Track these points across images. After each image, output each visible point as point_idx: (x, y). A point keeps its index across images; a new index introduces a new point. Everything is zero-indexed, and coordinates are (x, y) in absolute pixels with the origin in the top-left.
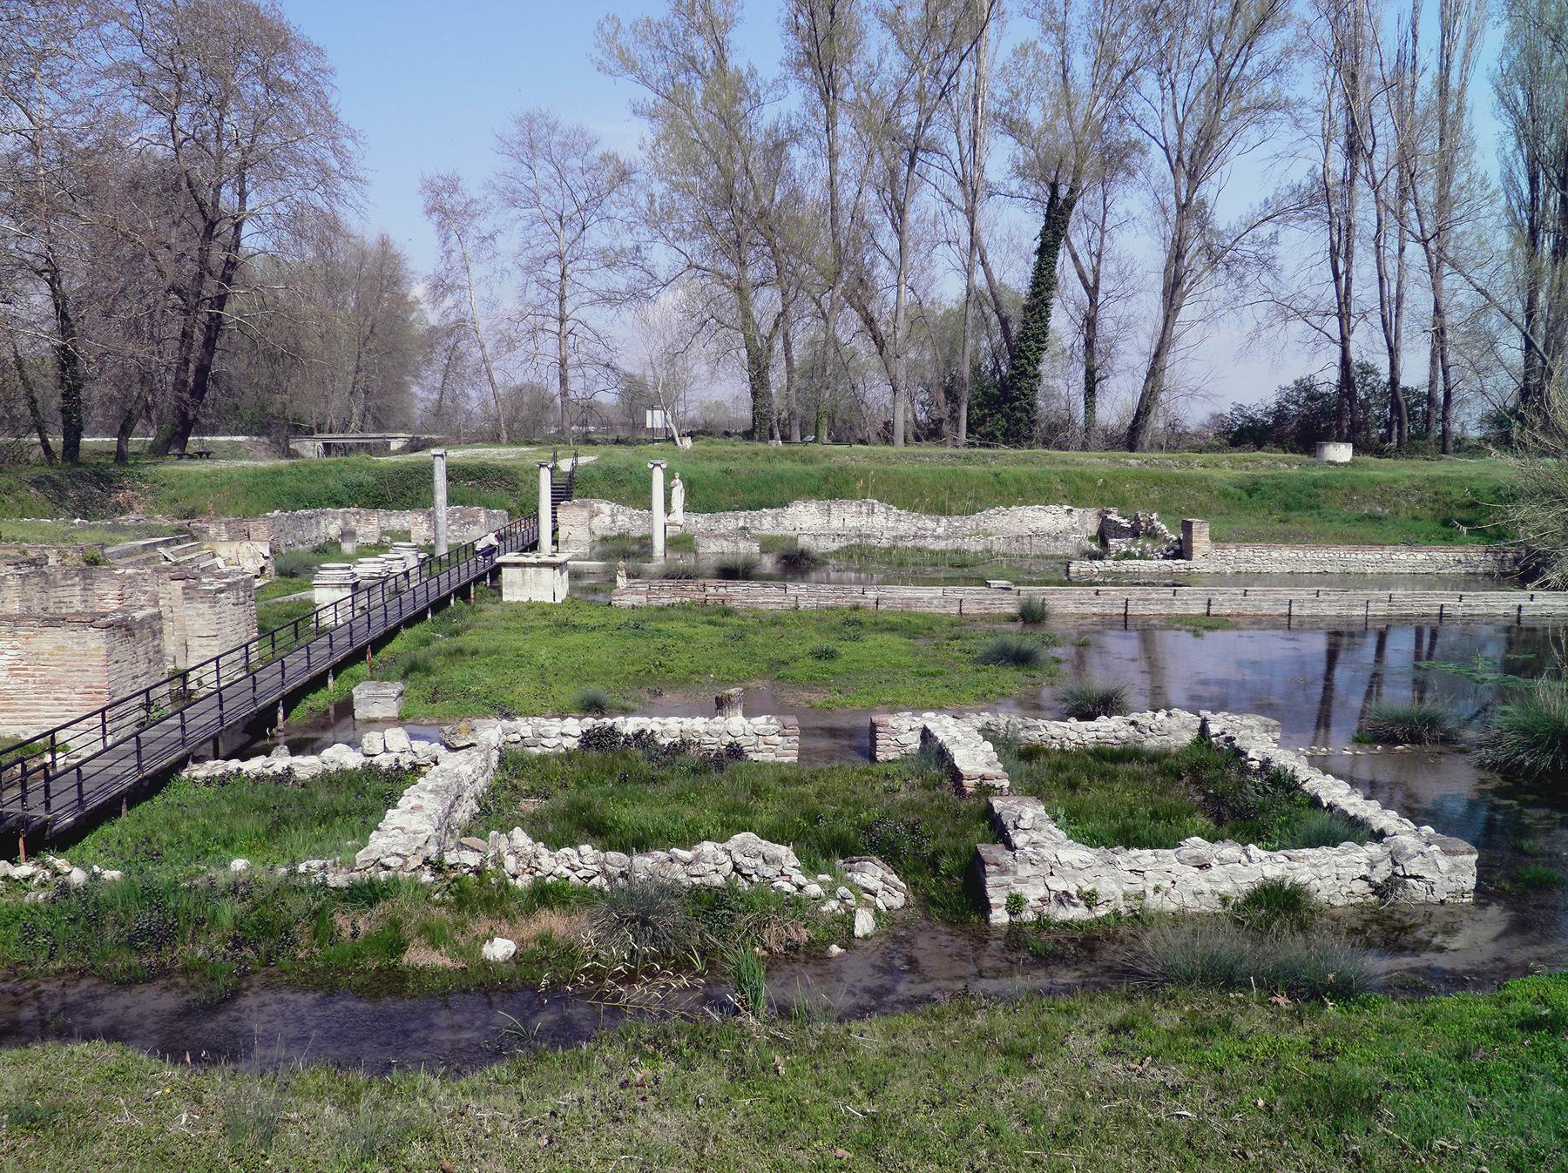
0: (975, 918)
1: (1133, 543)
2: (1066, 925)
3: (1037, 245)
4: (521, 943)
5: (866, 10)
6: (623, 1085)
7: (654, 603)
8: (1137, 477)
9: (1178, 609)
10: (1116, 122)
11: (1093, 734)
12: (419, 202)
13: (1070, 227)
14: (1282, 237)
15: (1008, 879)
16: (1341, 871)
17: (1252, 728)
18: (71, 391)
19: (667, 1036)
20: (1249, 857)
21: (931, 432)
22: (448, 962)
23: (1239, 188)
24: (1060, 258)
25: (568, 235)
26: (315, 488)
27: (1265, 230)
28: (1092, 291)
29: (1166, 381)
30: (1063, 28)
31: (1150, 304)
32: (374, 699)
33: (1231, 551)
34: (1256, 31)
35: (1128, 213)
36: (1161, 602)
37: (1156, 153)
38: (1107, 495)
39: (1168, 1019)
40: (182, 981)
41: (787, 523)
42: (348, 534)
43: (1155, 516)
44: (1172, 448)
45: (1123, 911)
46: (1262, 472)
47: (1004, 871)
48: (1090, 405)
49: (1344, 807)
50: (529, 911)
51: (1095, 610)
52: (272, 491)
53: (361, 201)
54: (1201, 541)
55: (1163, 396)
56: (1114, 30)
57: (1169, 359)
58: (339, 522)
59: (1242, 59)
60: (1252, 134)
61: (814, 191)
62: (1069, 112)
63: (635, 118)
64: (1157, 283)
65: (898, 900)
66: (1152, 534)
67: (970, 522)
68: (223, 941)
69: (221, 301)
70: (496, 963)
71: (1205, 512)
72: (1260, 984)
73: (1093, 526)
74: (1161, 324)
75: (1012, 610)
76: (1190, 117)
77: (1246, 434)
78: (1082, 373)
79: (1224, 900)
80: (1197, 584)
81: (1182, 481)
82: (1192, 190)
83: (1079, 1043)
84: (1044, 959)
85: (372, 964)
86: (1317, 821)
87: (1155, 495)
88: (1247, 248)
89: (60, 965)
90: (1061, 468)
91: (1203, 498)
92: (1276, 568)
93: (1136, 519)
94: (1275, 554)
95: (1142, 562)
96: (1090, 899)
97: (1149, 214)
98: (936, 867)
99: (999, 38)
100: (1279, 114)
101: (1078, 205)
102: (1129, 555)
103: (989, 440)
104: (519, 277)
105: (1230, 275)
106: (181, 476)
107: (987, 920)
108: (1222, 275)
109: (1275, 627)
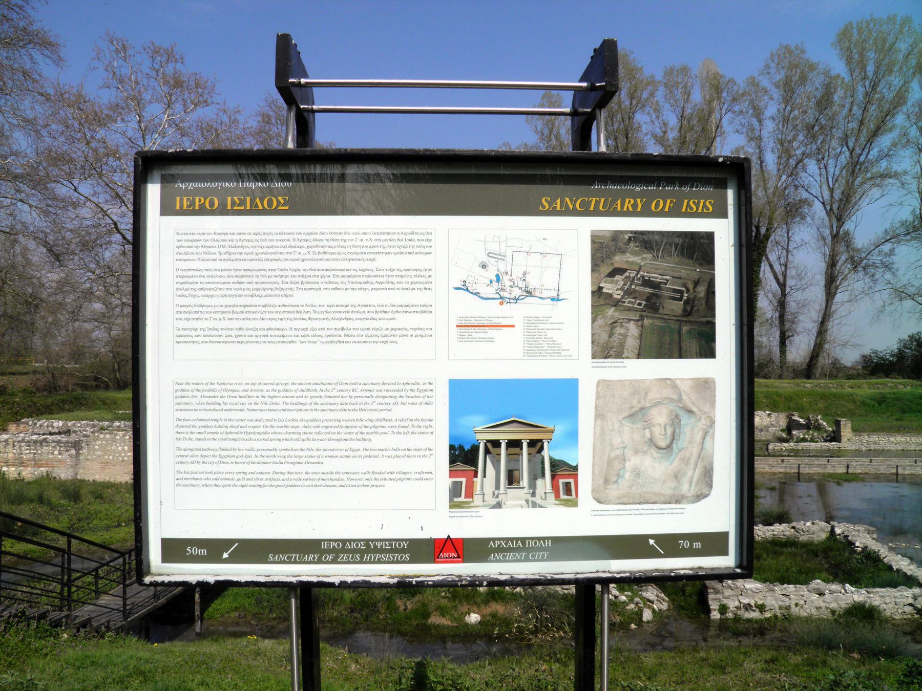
0: (703, 616)
1: (807, 433)
2: (749, 621)
4: (483, 616)
5: (647, 134)
6: (537, 670)
8: (810, 394)
9: (830, 470)
10: (793, 189)
11: (771, 533)
13: (768, 250)
14: (897, 251)
15: (720, 596)
16: (897, 600)
17: (859, 531)
19: (555, 653)
20: (845, 590)
22: (449, 623)
23: (869, 221)
24: (763, 268)
27: (886, 247)
28: (782, 286)
29: (828, 337)
30: (760, 138)
31: (817, 293)
33: (865, 438)
34: (875, 133)
35: (802, 240)
36: (819, 466)
37: (818, 206)
38: (792, 405)
39: (795, 659)
40: (329, 625)
43: (819, 417)
44: (832, 376)
45: (779, 615)
46: (887, 390)
47: (717, 592)
48: (783, 351)
49: (905, 571)
50: (486, 602)
54: (846, 431)
55: (827, 346)
56: (789, 138)
59: (866, 150)
60: (875, 192)
62: (765, 185)
64: (821, 280)
65: (665, 606)
66: (818, 428)
68: (345, 609)
70: (472, 625)
71: (850, 415)
72: (844, 647)
73: (783, 423)
74: (824, 304)
76: (837, 185)
77: (875, 367)
78: (778, 333)
79: (833, 612)
80: (844, 456)
81: (837, 397)
82: (839, 227)
83: (748, 665)
84: (737, 634)
85: (415, 623)
86: (886, 576)
87: (821, 405)
88: (875, 258)
89: (274, 615)
90: (765, 389)
91: (850, 406)
92: (893, 448)
93: (808, 419)
94: (892, 439)
95: (812, 444)
96: (761, 608)
97: (814, 241)
98: (684, 592)
99: (722, 146)
100: (891, 181)
101: (772, 238)
102: (804, 440)
105: (866, 274)
107: (709, 617)
108: (861, 274)
109: (888, 481)
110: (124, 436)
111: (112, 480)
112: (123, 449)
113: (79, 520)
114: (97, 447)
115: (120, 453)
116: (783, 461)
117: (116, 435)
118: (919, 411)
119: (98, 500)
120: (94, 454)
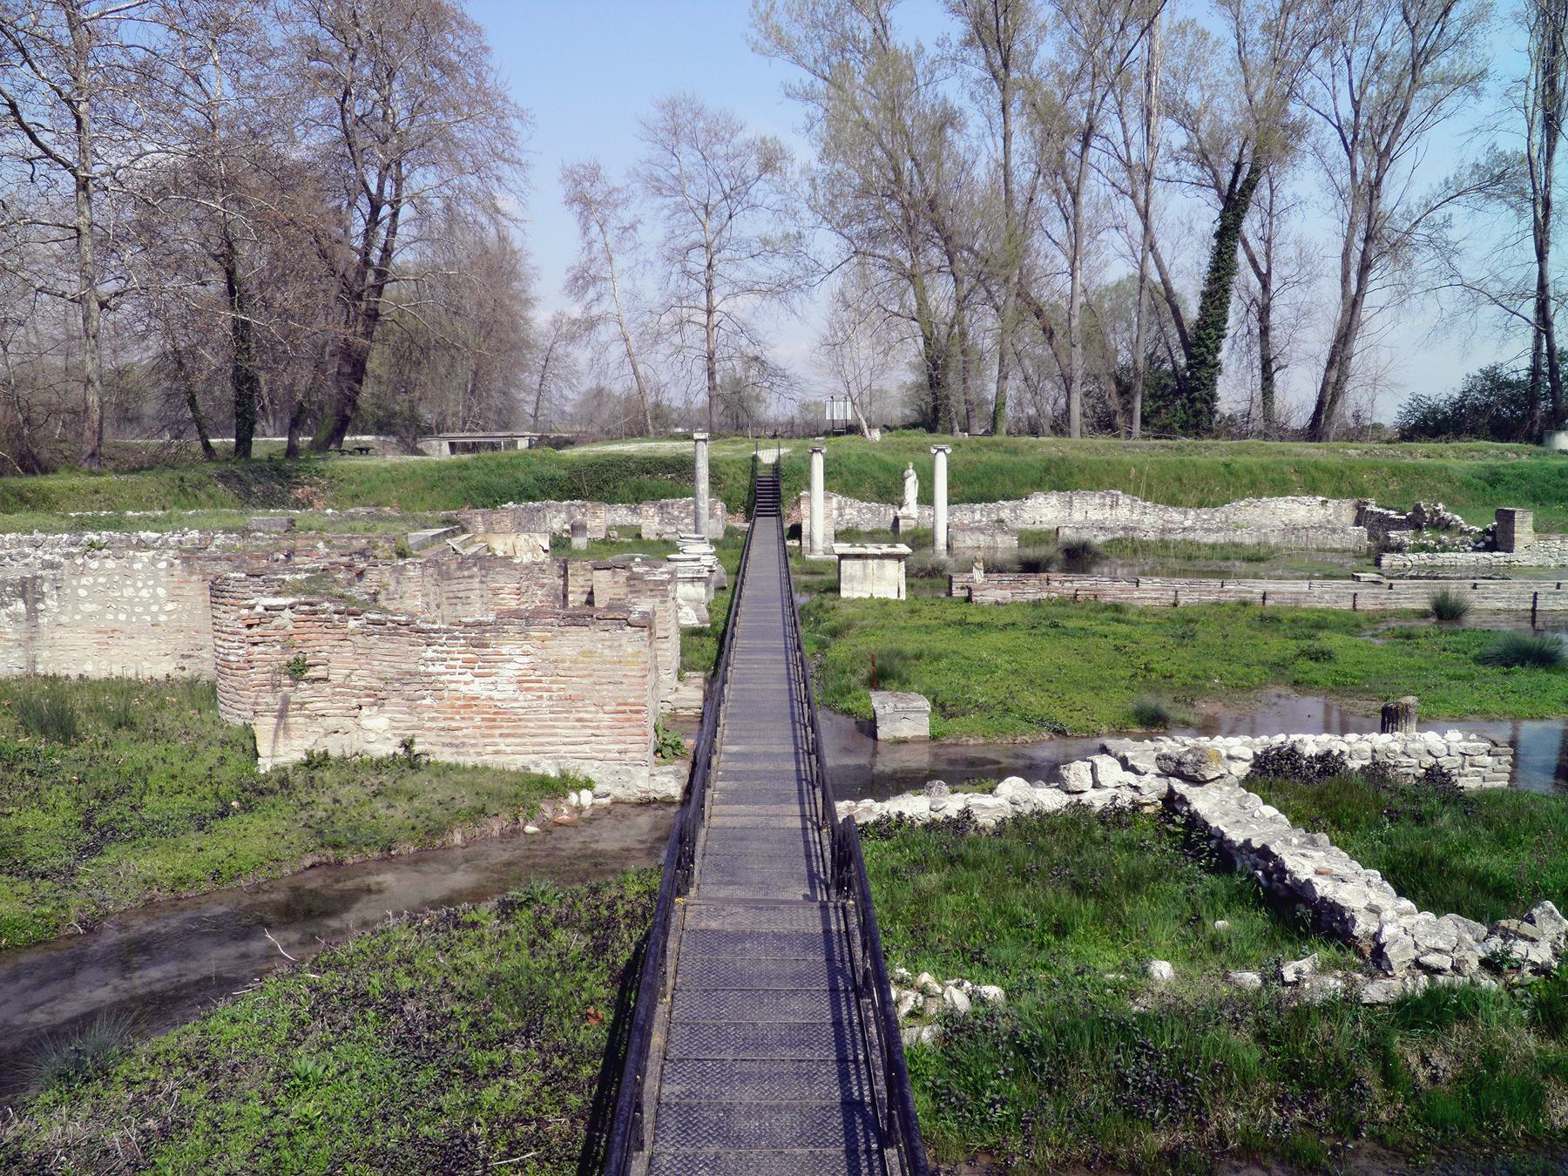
3: (1217, 227)
7: (1018, 598)
12: (560, 192)
18: (244, 382)
21: (1105, 424)
23: (1425, 165)
25: (714, 224)
26: (504, 481)
32: (904, 714)
41: (1026, 516)
42: (577, 529)
51: (1500, 605)
52: (460, 485)
53: (523, 186)
54: (1524, 529)
57: (1357, 346)
58: (563, 515)
61: (981, 173)
63: (790, 101)
67: (1219, 515)
69: (379, 290)
75: (1423, 604)
77: (1431, 425)
103: (1164, 431)
104: (660, 269)
106: (360, 471)
110: (153, 561)
111: (131, 673)
112: (154, 596)
113: (103, 797)
114: (82, 592)
115: (147, 606)
116: (1475, 587)
117: (133, 559)
118: (1562, 500)
119: (123, 732)
120: (77, 611)
